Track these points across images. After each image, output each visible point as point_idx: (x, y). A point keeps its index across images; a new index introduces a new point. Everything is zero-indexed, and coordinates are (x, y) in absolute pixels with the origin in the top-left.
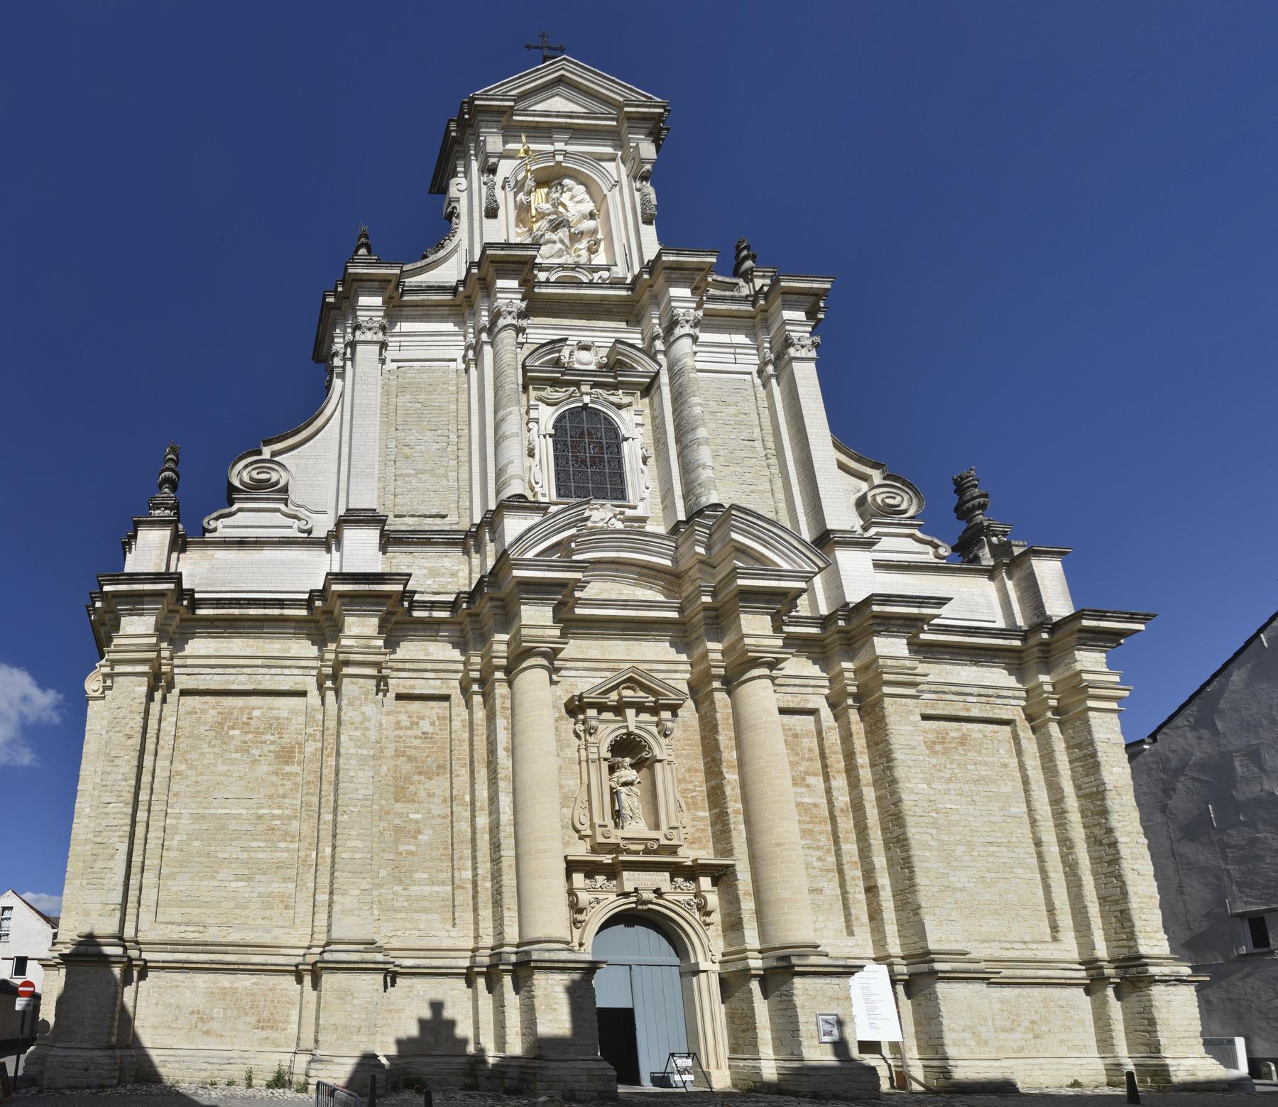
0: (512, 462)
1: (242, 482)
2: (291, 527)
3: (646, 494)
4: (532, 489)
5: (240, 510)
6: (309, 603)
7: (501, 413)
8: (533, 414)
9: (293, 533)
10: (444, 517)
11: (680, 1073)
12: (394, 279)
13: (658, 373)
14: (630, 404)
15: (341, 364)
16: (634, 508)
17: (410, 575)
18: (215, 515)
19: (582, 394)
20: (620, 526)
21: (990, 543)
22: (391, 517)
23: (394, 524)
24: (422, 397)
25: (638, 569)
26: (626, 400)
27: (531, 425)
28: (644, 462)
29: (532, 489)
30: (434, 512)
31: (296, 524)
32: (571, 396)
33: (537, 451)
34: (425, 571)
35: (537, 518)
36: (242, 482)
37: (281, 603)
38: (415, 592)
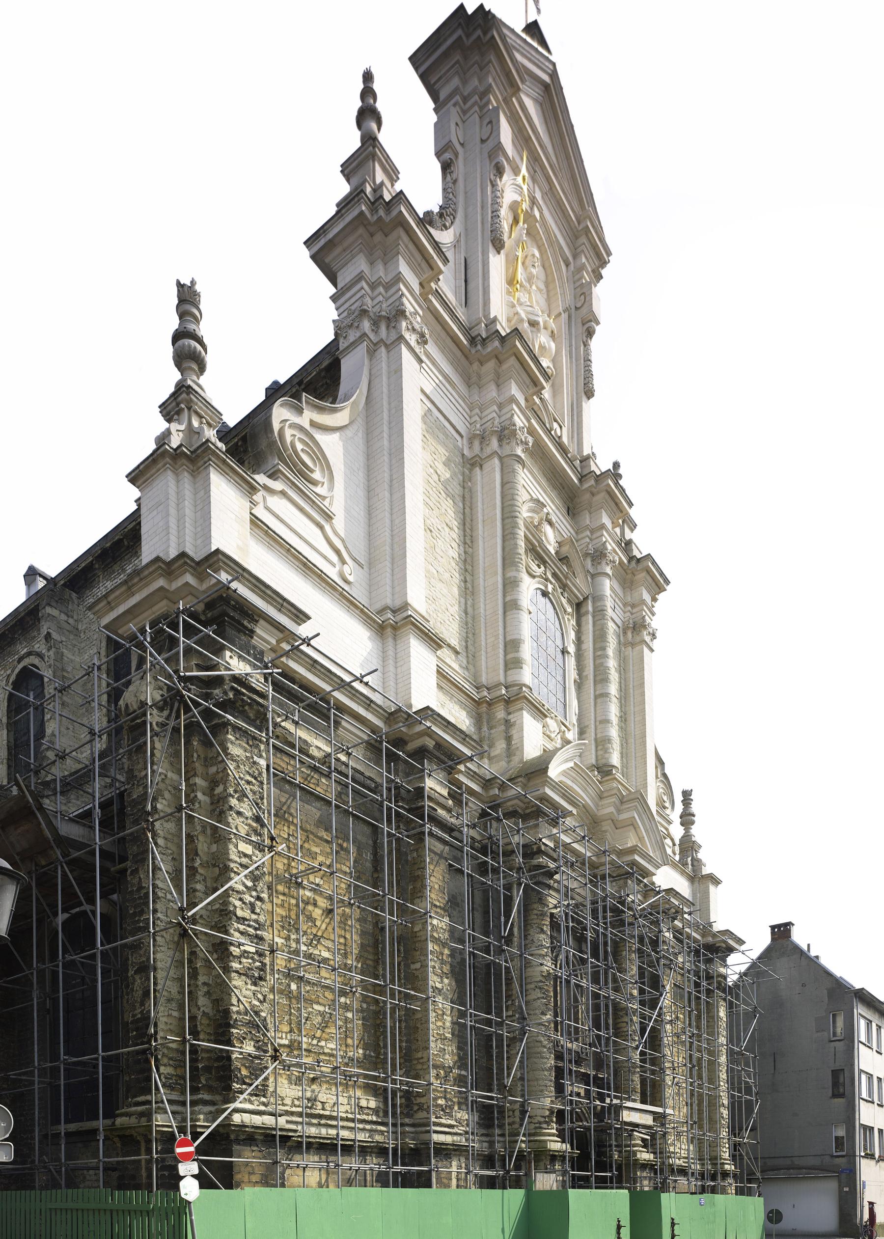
2: (334, 565)
5: (283, 493)
17: (309, 618)
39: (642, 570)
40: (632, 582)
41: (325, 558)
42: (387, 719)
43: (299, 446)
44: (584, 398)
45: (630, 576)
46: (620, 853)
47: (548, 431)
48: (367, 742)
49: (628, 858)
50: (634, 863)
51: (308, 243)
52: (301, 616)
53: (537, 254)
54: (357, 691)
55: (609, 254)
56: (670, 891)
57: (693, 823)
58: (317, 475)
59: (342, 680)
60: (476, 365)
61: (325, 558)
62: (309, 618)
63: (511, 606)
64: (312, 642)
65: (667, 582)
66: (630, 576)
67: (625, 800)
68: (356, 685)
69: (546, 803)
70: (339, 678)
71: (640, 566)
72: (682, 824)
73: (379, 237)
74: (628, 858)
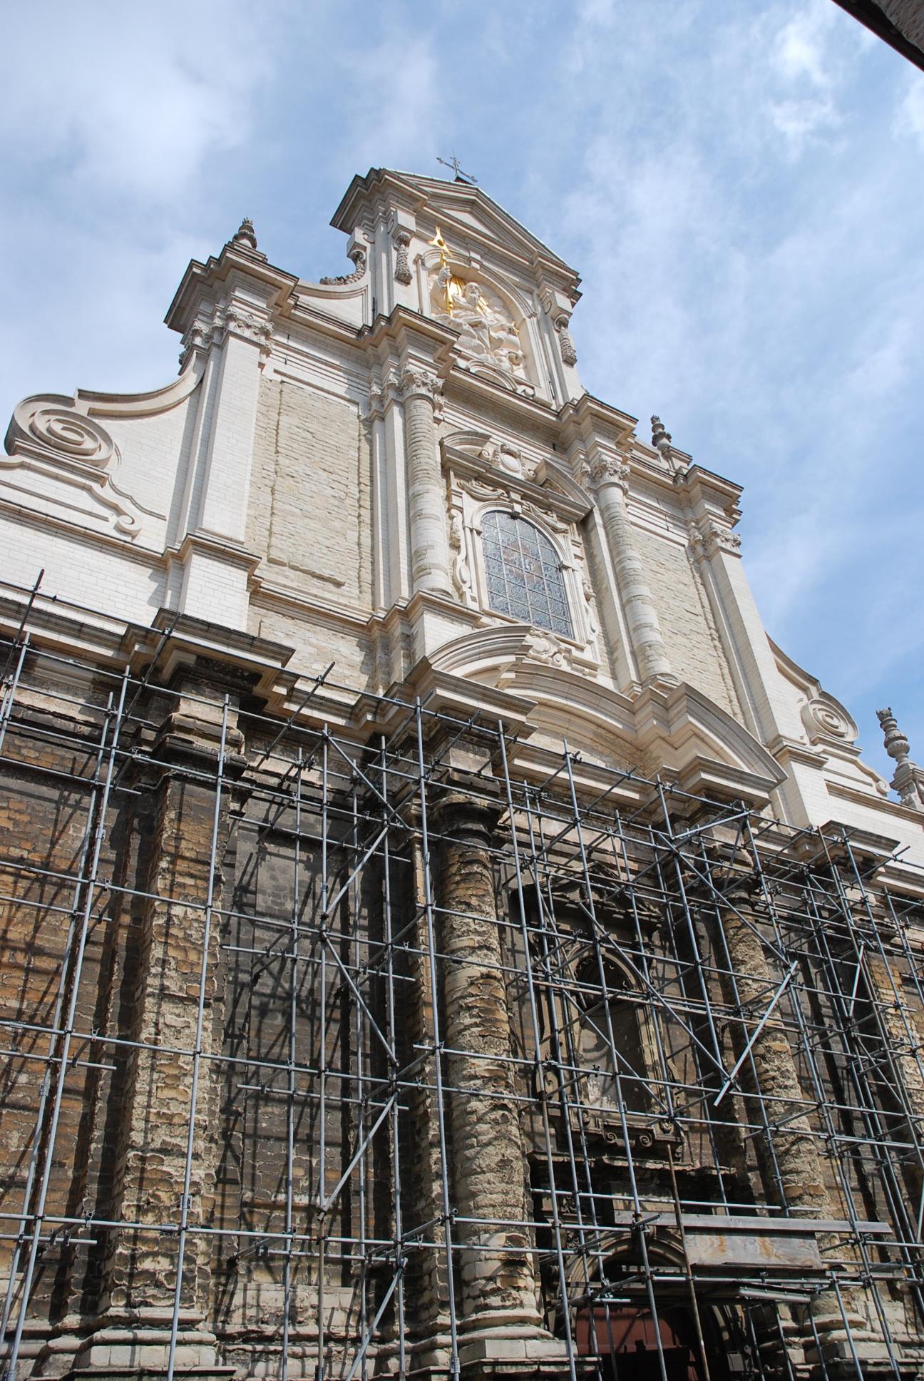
0: (432, 547)
1: (32, 428)
2: (106, 520)
3: (593, 637)
4: (458, 588)
5: (22, 466)
6: (121, 644)
7: (418, 487)
8: (455, 501)
9: (107, 528)
10: (339, 584)
11: (499, 1289)
12: (285, 289)
13: (591, 511)
14: (565, 532)
15: (314, 1300)
16: (582, 649)
17: (293, 651)
18: (371, 1151)
19: (513, 501)
20: (565, 667)
21: (691, 870)
22: (263, 564)
23: (271, 577)
24: (313, 427)
25: (594, 727)
26: (561, 525)
27: (454, 512)
28: (588, 600)
29: (458, 588)
30: (326, 573)
31: (113, 519)
32: (499, 499)
33: (462, 543)
34: (312, 650)
35: (464, 630)
36: (32, 428)
37: (79, 630)
38: (297, 677)
39: (694, 483)
40: (690, 500)
41: (90, 514)
42: (120, 644)
43: (57, 427)
44: (564, 367)
45: (683, 495)
46: (678, 778)
47: (513, 393)
48: (94, 682)
49: (692, 782)
50: (710, 790)
51: (165, 321)
52: (285, 653)
53: (474, 284)
54: (323, 698)
55: (576, 274)
56: (832, 827)
57: (907, 749)
58: (88, 444)
59: (20, 605)
60: (370, 350)
61: (90, 514)
62: (293, 651)
63: (414, 517)
64: (328, 679)
65: (741, 489)
66: (683, 495)
67: (670, 703)
68: (320, 691)
69: (452, 712)
70: (13, 602)
71: (690, 481)
72: (891, 755)
73: (217, 284)
74: (692, 782)
